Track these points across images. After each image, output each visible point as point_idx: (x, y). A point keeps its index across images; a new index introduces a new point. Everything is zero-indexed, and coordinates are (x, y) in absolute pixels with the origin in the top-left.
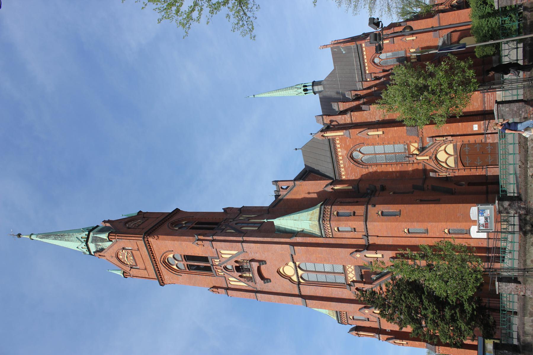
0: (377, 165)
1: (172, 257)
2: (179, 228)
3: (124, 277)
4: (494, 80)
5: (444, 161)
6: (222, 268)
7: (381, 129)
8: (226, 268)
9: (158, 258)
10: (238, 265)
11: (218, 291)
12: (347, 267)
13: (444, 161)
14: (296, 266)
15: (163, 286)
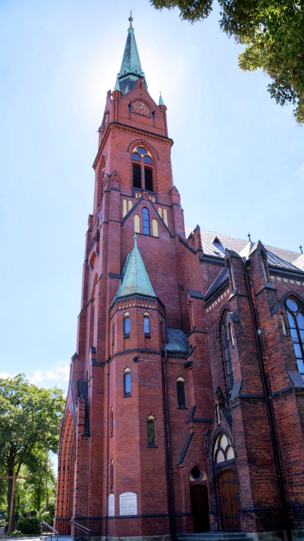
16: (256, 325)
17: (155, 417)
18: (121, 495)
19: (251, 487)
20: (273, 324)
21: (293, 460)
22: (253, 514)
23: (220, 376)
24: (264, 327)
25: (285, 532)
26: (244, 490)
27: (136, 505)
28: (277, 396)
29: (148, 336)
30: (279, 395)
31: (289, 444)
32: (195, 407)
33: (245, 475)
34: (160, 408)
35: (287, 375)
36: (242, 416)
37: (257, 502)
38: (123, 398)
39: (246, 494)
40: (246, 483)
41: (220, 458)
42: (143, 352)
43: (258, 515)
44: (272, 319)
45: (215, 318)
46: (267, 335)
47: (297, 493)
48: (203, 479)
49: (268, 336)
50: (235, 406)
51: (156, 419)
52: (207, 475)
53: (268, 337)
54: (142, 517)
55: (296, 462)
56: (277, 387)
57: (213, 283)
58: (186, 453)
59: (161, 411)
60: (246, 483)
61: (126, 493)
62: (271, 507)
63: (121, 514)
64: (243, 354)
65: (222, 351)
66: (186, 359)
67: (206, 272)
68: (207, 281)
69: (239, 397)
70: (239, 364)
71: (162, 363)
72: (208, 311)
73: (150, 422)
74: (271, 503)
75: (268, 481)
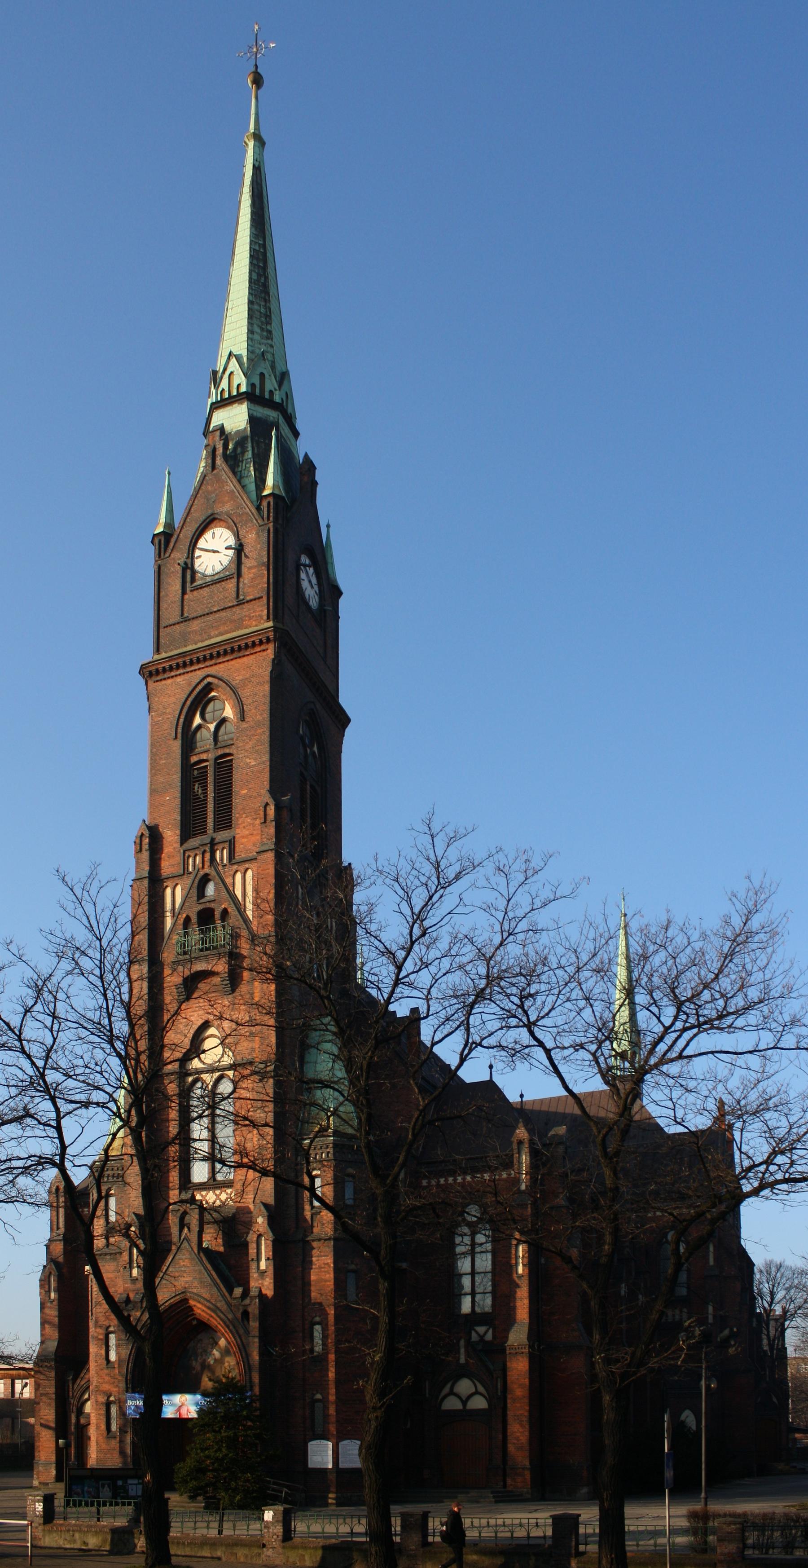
0: (172, 550)
1: (225, 715)
2: (302, 738)
3: (155, 536)
4: (554, 1518)
5: (456, 1390)
6: (207, 870)
7: (527, 1271)
8: (204, 880)
9: (221, 669)
10: (217, 914)
11: (144, 851)
12: (229, 1191)
13: (456, 1390)
14: (224, 1069)
15: (140, 673)
61: (318, 1441)
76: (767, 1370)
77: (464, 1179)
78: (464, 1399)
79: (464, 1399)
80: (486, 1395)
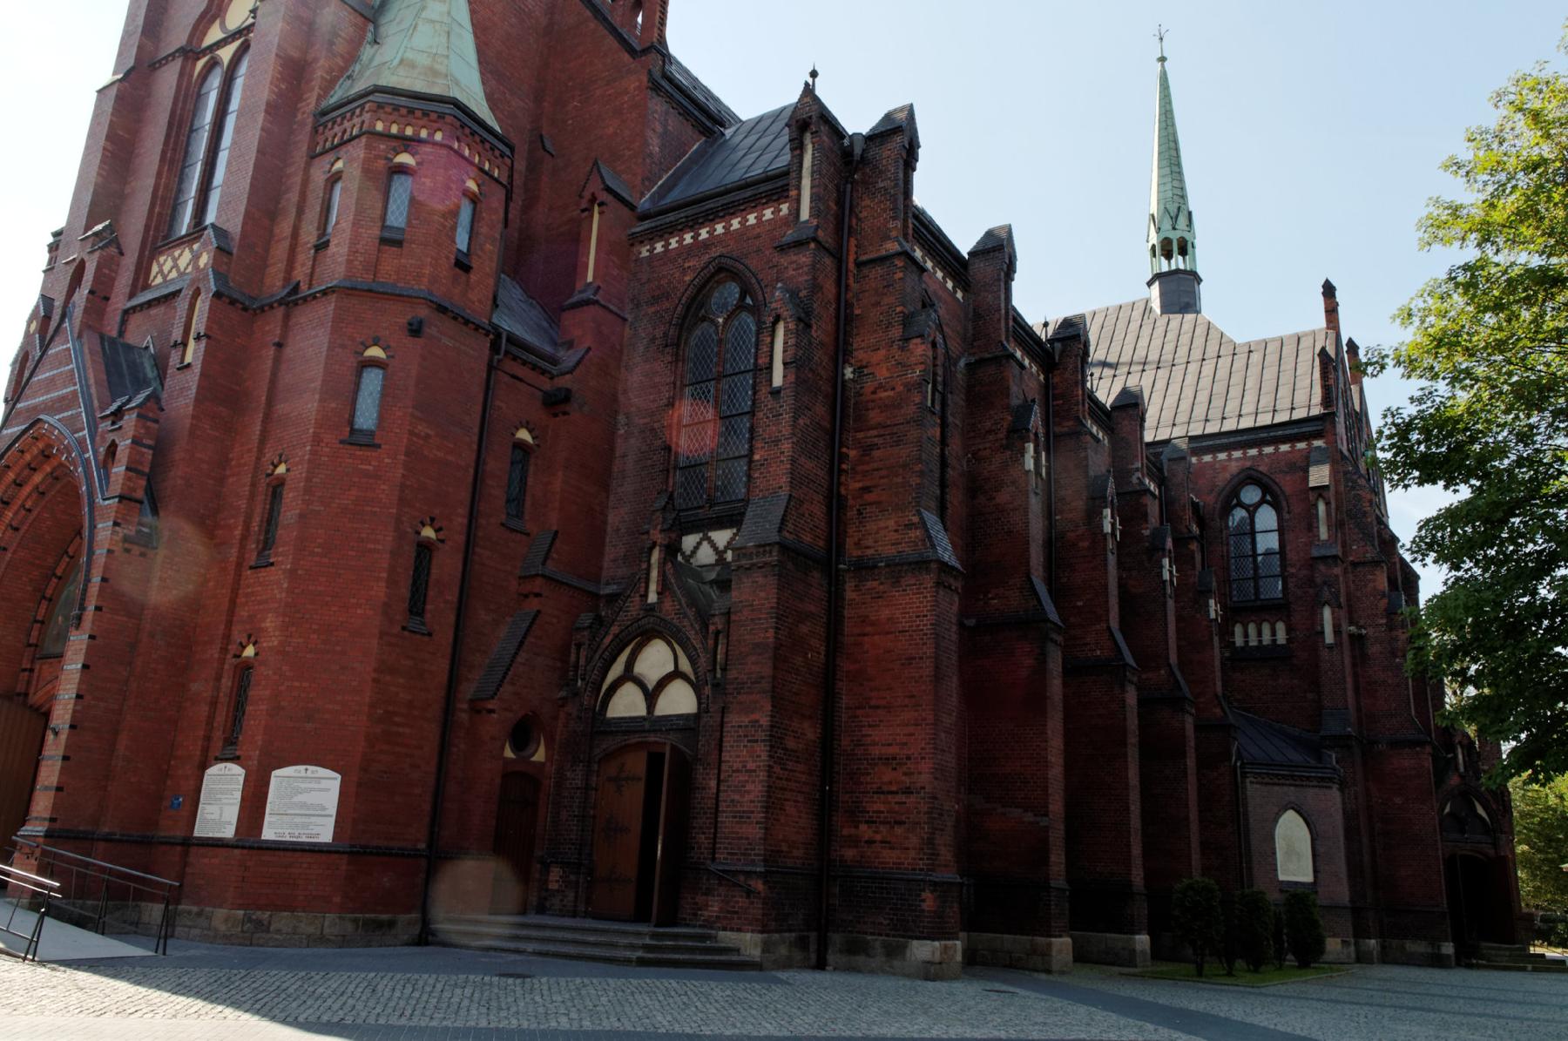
16: (841, 351)
17: (442, 535)
18: (275, 773)
19: (767, 807)
20: (905, 366)
21: (876, 751)
22: (759, 885)
23: (649, 462)
24: (864, 364)
25: (813, 935)
26: (731, 812)
27: (333, 810)
28: (864, 568)
29: (462, 265)
30: (875, 567)
31: (877, 707)
32: (556, 533)
33: (747, 771)
34: (460, 511)
35: (915, 519)
36: (775, 600)
37: (772, 851)
38: (341, 442)
39: (737, 823)
40: (748, 792)
41: (627, 704)
42: (442, 309)
43: (770, 888)
44: (902, 349)
45: (670, 282)
46: (872, 389)
47: (870, 842)
48: (534, 759)
49: (874, 393)
50: (753, 565)
51: (442, 541)
52: (547, 749)
53: (874, 396)
54: (351, 853)
55: (888, 759)
56: (870, 542)
57: (670, 172)
58: (508, 669)
59: (460, 521)
60: (748, 792)
61: (302, 768)
62: (797, 868)
63: (269, 834)
64: (801, 422)
65: (675, 388)
66: (552, 378)
67: (659, 129)
68: (655, 160)
69: (778, 543)
70: (786, 446)
71: (491, 368)
72: (645, 254)
73: (425, 548)
74: (797, 857)
75: (800, 798)
76: (1460, 750)
77: (651, 251)
78: (650, 687)
79: (650, 687)
80: (693, 677)
